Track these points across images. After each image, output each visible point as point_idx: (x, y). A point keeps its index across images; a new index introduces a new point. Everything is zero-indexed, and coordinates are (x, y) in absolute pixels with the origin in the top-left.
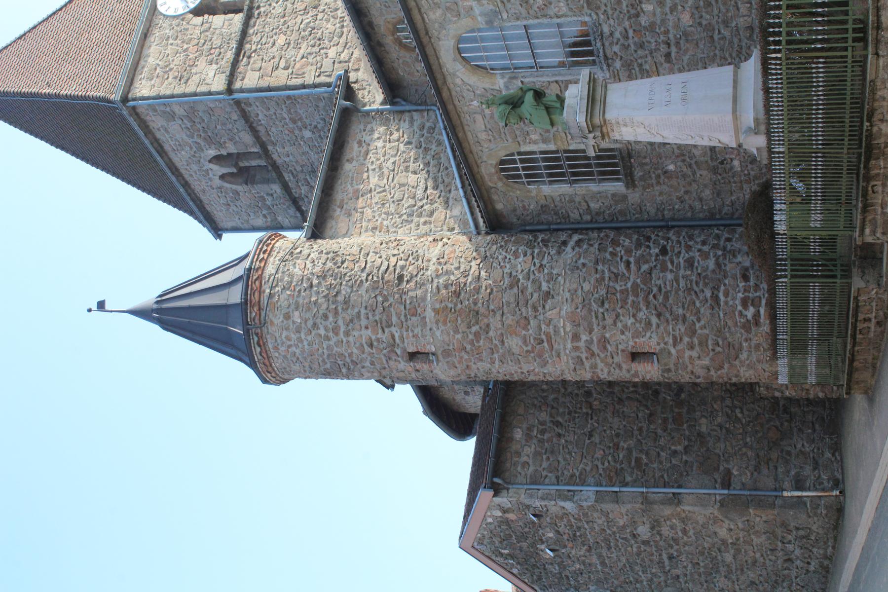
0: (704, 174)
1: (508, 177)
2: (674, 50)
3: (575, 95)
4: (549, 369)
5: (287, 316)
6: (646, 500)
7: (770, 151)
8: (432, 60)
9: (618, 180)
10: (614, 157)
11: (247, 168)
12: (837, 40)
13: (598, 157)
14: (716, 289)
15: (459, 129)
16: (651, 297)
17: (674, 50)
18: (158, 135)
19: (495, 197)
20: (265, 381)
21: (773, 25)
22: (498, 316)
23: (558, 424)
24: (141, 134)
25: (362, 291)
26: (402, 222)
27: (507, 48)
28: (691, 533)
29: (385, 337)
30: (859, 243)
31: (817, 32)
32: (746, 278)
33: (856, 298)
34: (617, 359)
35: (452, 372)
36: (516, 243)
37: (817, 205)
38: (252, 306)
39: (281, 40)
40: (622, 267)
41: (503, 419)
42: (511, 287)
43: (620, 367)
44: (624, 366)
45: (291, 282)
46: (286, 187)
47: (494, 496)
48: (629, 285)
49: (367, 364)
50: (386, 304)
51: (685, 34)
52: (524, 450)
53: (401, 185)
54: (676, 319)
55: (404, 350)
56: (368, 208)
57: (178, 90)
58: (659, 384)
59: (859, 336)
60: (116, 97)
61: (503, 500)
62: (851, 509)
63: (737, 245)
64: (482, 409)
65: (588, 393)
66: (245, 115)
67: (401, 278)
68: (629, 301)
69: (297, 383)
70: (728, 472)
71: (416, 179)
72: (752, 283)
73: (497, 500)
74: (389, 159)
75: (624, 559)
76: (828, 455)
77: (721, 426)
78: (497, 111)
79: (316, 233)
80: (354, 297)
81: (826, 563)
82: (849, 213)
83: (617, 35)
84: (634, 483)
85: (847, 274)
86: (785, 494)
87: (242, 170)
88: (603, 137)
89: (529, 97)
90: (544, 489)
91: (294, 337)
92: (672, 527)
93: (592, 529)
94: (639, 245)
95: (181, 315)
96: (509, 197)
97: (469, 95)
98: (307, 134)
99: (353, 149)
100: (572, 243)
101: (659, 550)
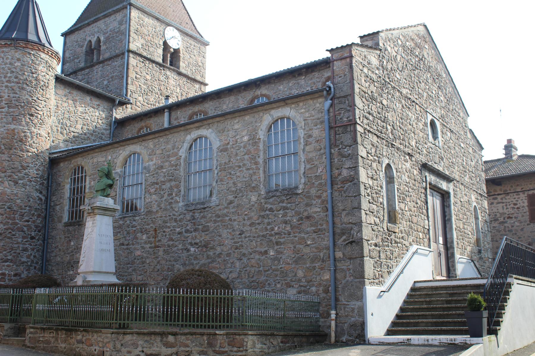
0: (68, 258)
1: (75, 170)
3: (109, 202)
5: (19, 60)
7: (73, 287)
8: (132, 141)
9: (69, 219)
10: (80, 218)
11: (93, 53)
14: (11, 261)
15: (99, 150)
16: (10, 231)
17: (125, 247)
18: (113, 16)
19: (66, 163)
22: (7, 159)
24: (115, 9)
25: (27, 97)
27: (133, 175)
30: (27, 326)
32: (15, 275)
36: (44, 170)
38: (25, 44)
39: (149, 77)
42: (22, 166)
45: (36, 64)
46: (82, 69)
48: (17, 221)
50: (19, 107)
51: (131, 252)
53: (77, 121)
56: (67, 105)
63: (32, 272)
66: (117, 56)
67: (32, 115)
68: (9, 221)
71: (78, 128)
74: (90, 117)
78: (106, 167)
79: (58, 79)
80: (24, 92)
82: (42, 322)
83: (134, 223)
87: (92, 50)
88: (89, 213)
89: (110, 182)
91: (8, 61)
94: (36, 227)
96: (65, 171)
98: (105, 82)
99: (96, 102)
100: (41, 196)
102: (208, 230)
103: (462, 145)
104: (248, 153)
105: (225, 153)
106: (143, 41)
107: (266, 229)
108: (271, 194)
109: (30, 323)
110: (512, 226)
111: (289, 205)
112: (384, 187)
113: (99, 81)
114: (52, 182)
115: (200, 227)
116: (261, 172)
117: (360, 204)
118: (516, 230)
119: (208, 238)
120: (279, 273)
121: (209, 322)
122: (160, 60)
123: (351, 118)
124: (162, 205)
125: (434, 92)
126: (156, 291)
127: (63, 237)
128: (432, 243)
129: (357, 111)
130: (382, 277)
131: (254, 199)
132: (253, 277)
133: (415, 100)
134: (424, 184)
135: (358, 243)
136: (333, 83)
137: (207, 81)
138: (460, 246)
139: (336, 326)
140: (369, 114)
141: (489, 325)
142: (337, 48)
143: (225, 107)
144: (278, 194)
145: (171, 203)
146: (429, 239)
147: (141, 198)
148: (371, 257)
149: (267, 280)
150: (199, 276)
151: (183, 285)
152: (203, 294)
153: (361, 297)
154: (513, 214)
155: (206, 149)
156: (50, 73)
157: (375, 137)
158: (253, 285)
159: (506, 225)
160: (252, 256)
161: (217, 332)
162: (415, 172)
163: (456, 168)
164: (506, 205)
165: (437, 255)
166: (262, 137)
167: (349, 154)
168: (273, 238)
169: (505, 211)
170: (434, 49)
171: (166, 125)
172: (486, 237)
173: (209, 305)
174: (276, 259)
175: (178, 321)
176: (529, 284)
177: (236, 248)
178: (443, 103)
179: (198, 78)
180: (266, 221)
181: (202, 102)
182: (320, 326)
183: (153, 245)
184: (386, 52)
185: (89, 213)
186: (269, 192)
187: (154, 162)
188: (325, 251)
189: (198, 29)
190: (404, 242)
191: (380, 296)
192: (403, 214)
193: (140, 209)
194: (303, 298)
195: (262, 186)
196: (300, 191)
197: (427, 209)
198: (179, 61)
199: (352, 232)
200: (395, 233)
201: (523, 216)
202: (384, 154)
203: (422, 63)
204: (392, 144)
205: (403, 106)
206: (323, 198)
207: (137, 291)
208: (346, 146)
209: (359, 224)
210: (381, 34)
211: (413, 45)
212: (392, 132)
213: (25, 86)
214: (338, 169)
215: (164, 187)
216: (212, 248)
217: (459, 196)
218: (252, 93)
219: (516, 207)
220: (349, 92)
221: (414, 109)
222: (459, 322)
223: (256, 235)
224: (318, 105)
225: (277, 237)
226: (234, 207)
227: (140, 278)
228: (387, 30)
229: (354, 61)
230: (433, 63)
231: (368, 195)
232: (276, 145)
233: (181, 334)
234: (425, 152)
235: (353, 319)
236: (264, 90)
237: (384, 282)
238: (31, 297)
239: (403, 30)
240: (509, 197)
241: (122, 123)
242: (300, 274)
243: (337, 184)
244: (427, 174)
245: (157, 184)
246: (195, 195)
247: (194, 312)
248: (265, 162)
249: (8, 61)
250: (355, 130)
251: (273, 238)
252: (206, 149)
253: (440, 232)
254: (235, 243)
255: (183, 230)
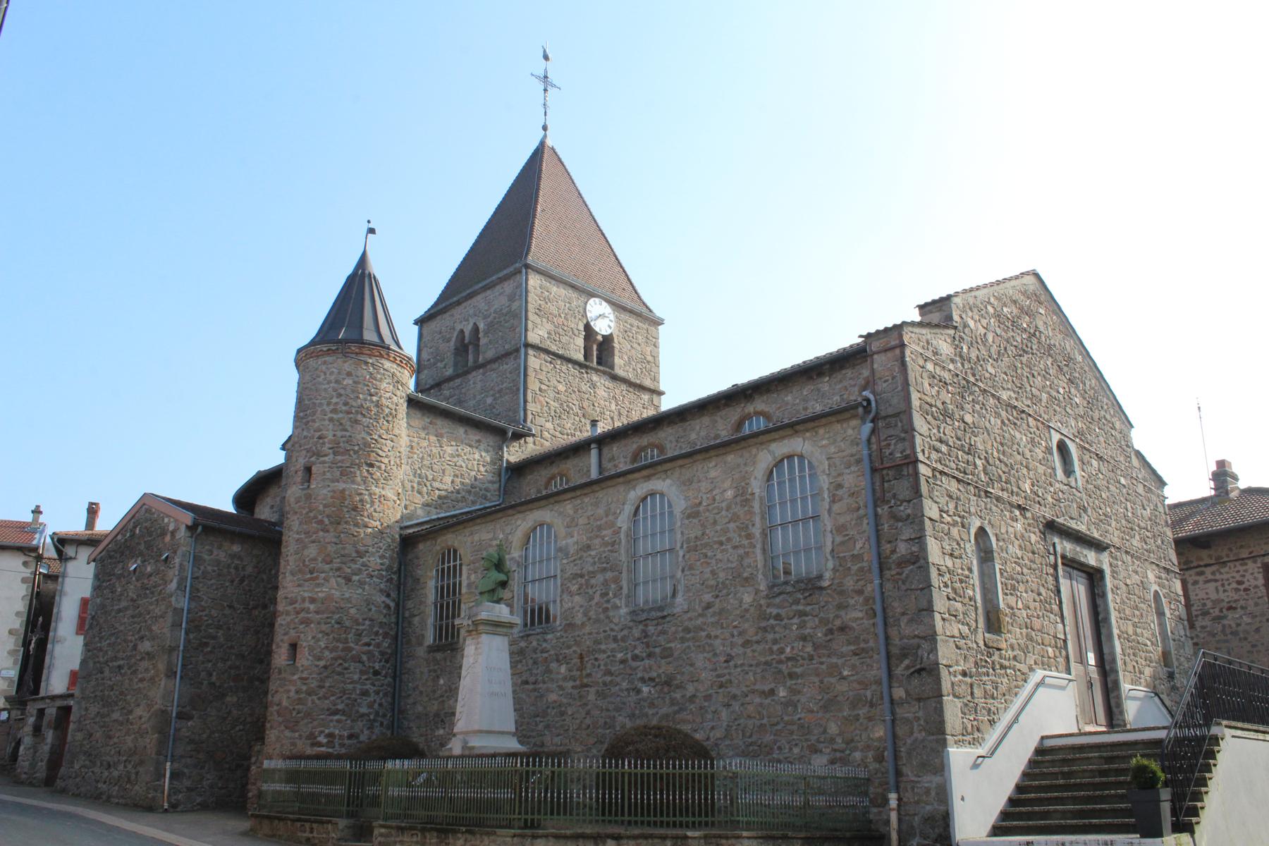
0: (434, 707)
1: (443, 555)
2: (531, 687)
3: (502, 612)
4: (289, 577)
5: (349, 374)
6: (172, 649)
7: (448, 758)
8: (537, 504)
9: (435, 640)
10: (453, 637)
11: (467, 351)
12: (526, 807)
13: (453, 626)
14: (344, 713)
17: (531, 687)
18: (498, 287)
19: (428, 543)
20: (299, 351)
21: (540, 762)
22: (334, 540)
23: (242, 581)
24: (501, 275)
25: (363, 435)
26: (413, 469)
27: (541, 561)
28: (140, 685)
29: (325, 449)
30: (375, 824)
31: (533, 793)
32: (351, 737)
33: (329, 822)
34: (292, 633)
35: (292, 500)
36: (391, 558)
37: (405, 792)
38: (360, 348)
39: (561, 388)
40: (366, 640)
41: (250, 537)
42: (357, 552)
43: (285, 634)
44: (286, 638)
46: (450, 379)
47: (187, 527)
49: (305, 433)
51: (542, 696)
52: (223, 552)
53: (444, 471)
54: (322, 680)
55: (314, 463)
56: (428, 443)
57: (530, 307)
58: (269, 664)
59: (299, 824)
60: (530, 260)
61: (182, 533)
62: (151, 817)
63: (377, 731)
64: (259, 520)
65: (265, 607)
66: (507, 354)
67: (372, 465)
69: (295, 376)
70: (190, 718)
71: (447, 483)
72: (346, 741)
73: (183, 528)
74: (464, 462)
75: (122, 628)
76: (199, 800)
77: (229, 713)
78: (493, 551)
79: (412, 402)
80: (359, 427)
81: (104, 797)
82: (397, 817)
83: (545, 645)
84: (188, 641)
85: (350, 815)
86: (168, 764)
87: (466, 346)
88: (469, 631)
89: (502, 577)
90: (189, 567)
91: (332, 378)
92: (147, 670)
93: (151, 604)
94: (382, 654)
95: (359, 289)
96: (427, 554)
97: (508, 530)
98: (489, 400)
99: (474, 435)
100: (388, 601)
101: (129, 658)
102: (671, 655)
103: (1123, 481)
104: (735, 518)
105: (695, 521)
106: (549, 326)
107: (771, 652)
108: (776, 589)
109: (378, 818)
110: (1238, 625)
111: (808, 608)
112: (975, 569)
113: (478, 397)
114: (406, 576)
115: (657, 650)
116: (758, 551)
117: (930, 602)
118: (1247, 632)
119: (671, 669)
120: (795, 727)
121: (674, 815)
122: (580, 357)
123: (908, 452)
124: (592, 614)
125: (1061, 391)
126: (585, 764)
127: (426, 670)
128: (1073, 664)
129: (918, 440)
130: (978, 730)
131: (748, 599)
132: (751, 736)
133: (1026, 409)
134: (1052, 558)
135: (930, 671)
136: (873, 392)
137: (662, 388)
138: (1130, 668)
139: (900, 820)
140: (941, 441)
141: (1174, 812)
142: (878, 332)
143: (693, 436)
144: (789, 589)
145: (606, 610)
146: (1067, 658)
147: (555, 602)
148: (955, 696)
149: (775, 742)
150: (656, 736)
151: (629, 753)
152: (666, 768)
153: (939, 767)
154: (1236, 601)
155: (662, 514)
156: (398, 393)
157: (954, 483)
158: (753, 751)
159: (1225, 622)
160: (748, 699)
161: (689, 834)
162: (1033, 538)
163: (1114, 524)
164: (1223, 585)
165: (1084, 687)
166: (757, 491)
167: (909, 516)
168: (783, 667)
169: (1222, 596)
170: (1056, 314)
171: (594, 474)
172: (1183, 647)
173: (674, 786)
174: (789, 704)
175: (623, 815)
176: (1261, 736)
177: (721, 686)
178: (1081, 408)
179: (647, 383)
180: (770, 636)
181: (654, 429)
182: (870, 821)
183: (578, 683)
184: (966, 330)
185: (469, 631)
186: (773, 586)
187: (575, 539)
188: (874, 687)
189: (643, 298)
190: (1018, 666)
191: (975, 766)
192: (1014, 614)
193: (555, 620)
194: (840, 771)
195: (760, 576)
196: (826, 584)
197: (1061, 602)
198: (613, 355)
199: (920, 652)
200: (999, 649)
201: (1256, 604)
202: (973, 510)
203: (1035, 341)
204: (986, 492)
205: (1003, 422)
206: (866, 594)
207: (553, 765)
208: (902, 502)
209: (932, 638)
210: (955, 300)
211: (1015, 311)
212: (985, 470)
213: (359, 417)
214: (890, 542)
215: (593, 581)
216: (678, 687)
217: (1122, 574)
218: (739, 410)
219: (1242, 587)
220: (903, 407)
221: (1025, 426)
222: (1122, 810)
223: (754, 663)
224: (850, 432)
225: (790, 664)
226: (714, 614)
227: (557, 740)
228: (965, 291)
229: (908, 352)
230: (1057, 339)
231: (946, 586)
232: (783, 504)
233: (629, 838)
234: (1050, 499)
235: (928, 808)
236: (759, 404)
237: (984, 739)
238: (380, 774)
239: (996, 287)
240: (1227, 569)
241: (519, 470)
242: (833, 729)
243: (889, 569)
244: (1056, 540)
245: (582, 576)
246: (649, 594)
247: (649, 798)
248: (764, 534)
249: (332, 378)
250: (916, 473)
251: (783, 667)
252: (662, 514)
253: (1089, 643)
254: (718, 676)
255: (629, 656)
